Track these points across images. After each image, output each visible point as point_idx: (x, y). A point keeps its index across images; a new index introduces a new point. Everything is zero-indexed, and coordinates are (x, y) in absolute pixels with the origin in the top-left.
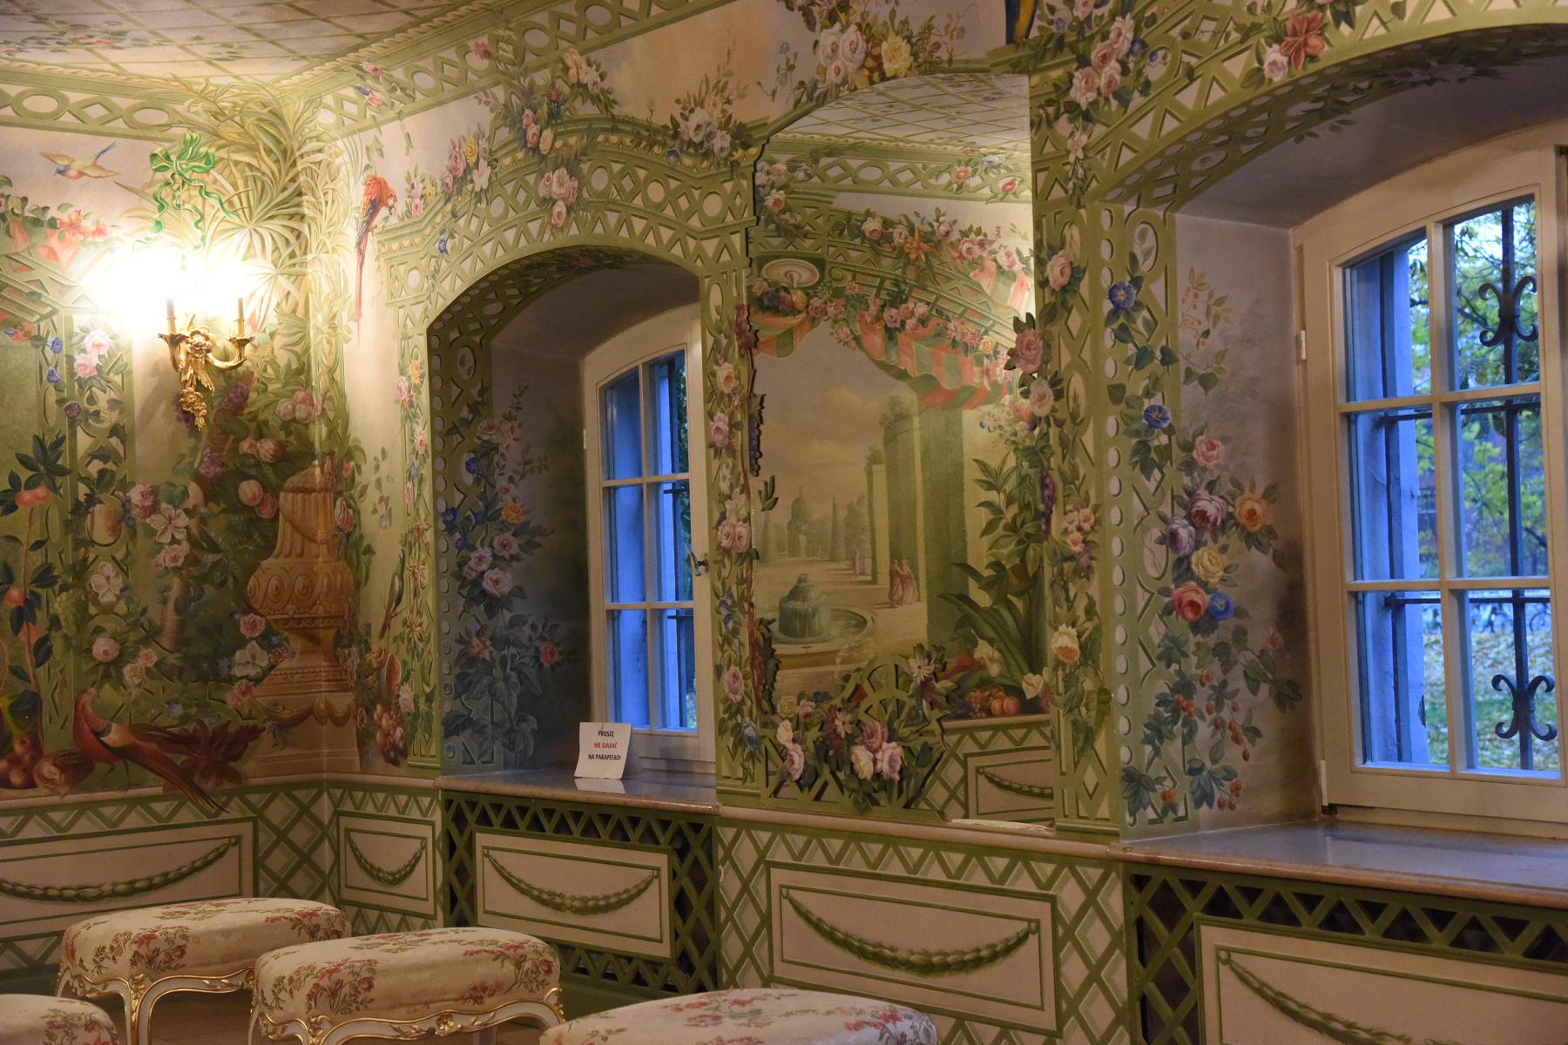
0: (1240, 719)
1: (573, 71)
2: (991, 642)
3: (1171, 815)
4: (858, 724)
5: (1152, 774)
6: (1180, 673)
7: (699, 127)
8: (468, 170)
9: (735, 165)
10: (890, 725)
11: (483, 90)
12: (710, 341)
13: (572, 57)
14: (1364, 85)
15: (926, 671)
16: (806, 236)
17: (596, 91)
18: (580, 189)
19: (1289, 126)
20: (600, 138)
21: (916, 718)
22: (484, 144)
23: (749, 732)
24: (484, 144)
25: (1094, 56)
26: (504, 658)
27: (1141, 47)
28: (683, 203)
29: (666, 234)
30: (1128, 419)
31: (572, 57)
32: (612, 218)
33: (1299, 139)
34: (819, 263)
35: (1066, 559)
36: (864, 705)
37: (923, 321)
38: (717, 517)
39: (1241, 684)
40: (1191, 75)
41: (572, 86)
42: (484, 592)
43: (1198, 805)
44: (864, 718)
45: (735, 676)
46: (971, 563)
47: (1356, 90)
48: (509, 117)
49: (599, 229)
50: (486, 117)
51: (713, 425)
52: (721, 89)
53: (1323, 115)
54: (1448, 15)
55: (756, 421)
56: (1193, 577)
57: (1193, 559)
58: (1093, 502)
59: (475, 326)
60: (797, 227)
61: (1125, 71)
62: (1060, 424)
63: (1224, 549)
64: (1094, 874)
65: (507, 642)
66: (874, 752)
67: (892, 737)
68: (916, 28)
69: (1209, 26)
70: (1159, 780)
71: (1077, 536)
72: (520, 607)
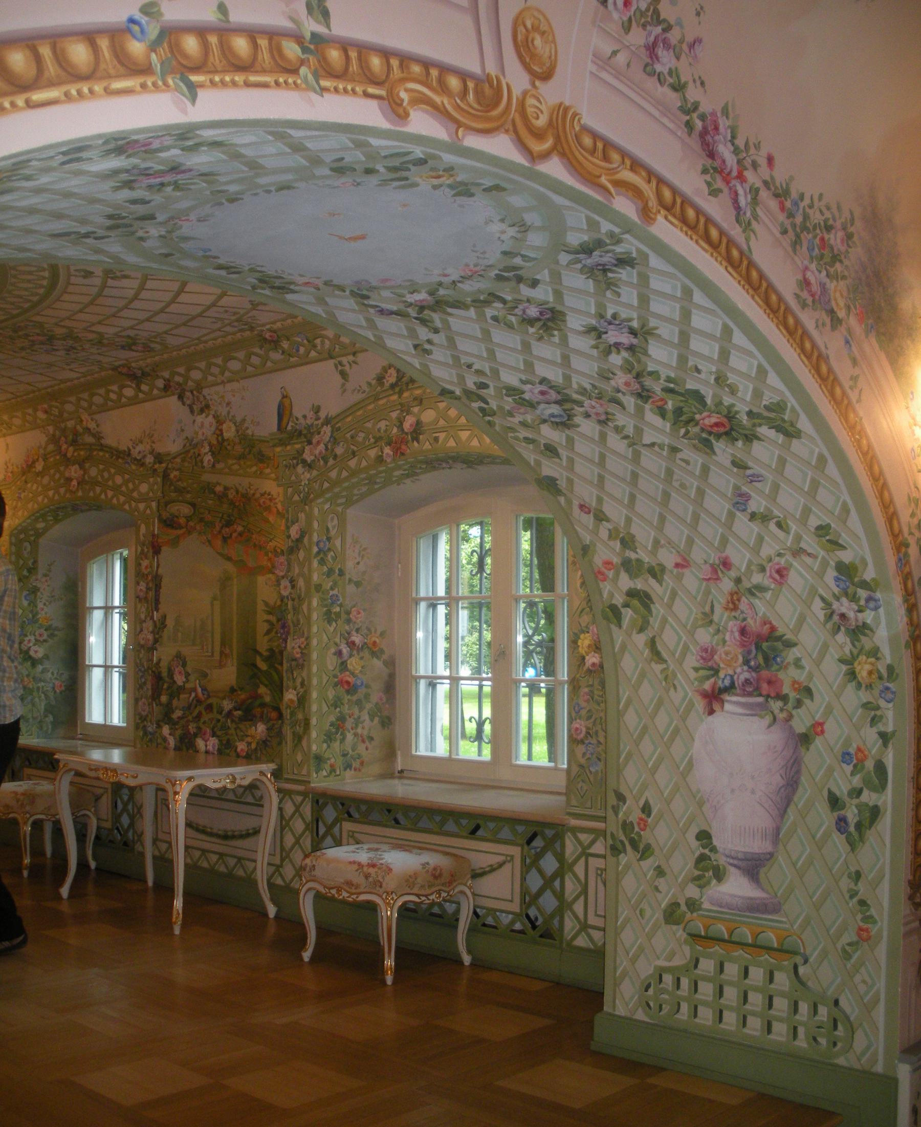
0: (365, 733)
1: (84, 423)
2: (266, 686)
3: (333, 774)
4: (199, 728)
5: (326, 756)
6: (340, 712)
7: (140, 452)
8: (34, 462)
9: (155, 470)
10: (213, 729)
11: (43, 427)
12: (139, 549)
13: (85, 416)
14: (424, 466)
15: (230, 706)
16: (188, 492)
17: (94, 432)
18: (84, 475)
19: (394, 479)
20: (95, 453)
21: (225, 728)
22: (42, 451)
23: (150, 729)
24: (42, 451)
25: (314, 441)
26: (38, 688)
27: (335, 441)
28: (131, 486)
29: (122, 499)
30: (323, 600)
31: (85, 416)
32: (98, 489)
33: (399, 484)
34: (193, 505)
35: (293, 660)
36: (202, 721)
37: (240, 534)
38: (138, 630)
39: (367, 717)
40: (354, 454)
41: (84, 429)
42: (30, 657)
43: (345, 769)
44: (201, 725)
45: (144, 704)
46: (258, 648)
47: (421, 468)
48: (54, 440)
49: (91, 494)
50: (43, 439)
51: (139, 588)
52: (151, 436)
53: (408, 476)
54: (455, 445)
55: (158, 587)
56: (348, 670)
57: (348, 662)
58: (306, 635)
59: (32, 533)
60: (184, 488)
61: (327, 449)
62: (293, 600)
63: (362, 658)
64: (299, 799)
65: (40, 680)
66: (206, 741)
67: (214, 734)
68: (238, 419)
69: (362, 435)
70: (329, 759)
71: (298, 650)
72: (47, 665)
